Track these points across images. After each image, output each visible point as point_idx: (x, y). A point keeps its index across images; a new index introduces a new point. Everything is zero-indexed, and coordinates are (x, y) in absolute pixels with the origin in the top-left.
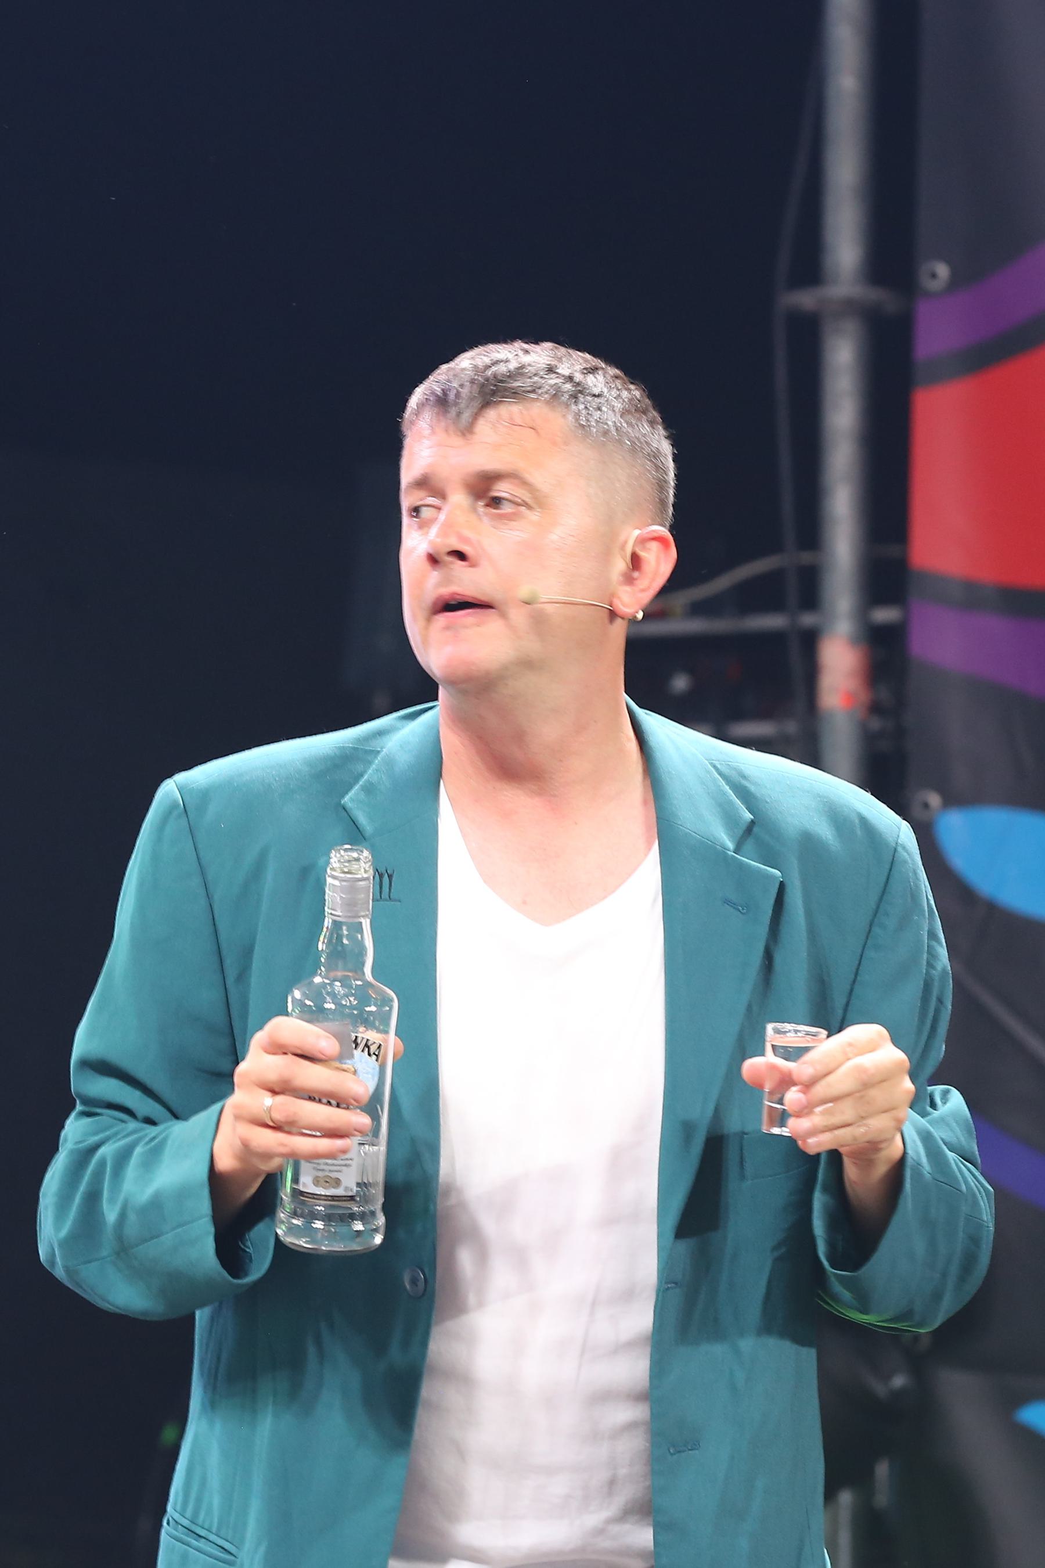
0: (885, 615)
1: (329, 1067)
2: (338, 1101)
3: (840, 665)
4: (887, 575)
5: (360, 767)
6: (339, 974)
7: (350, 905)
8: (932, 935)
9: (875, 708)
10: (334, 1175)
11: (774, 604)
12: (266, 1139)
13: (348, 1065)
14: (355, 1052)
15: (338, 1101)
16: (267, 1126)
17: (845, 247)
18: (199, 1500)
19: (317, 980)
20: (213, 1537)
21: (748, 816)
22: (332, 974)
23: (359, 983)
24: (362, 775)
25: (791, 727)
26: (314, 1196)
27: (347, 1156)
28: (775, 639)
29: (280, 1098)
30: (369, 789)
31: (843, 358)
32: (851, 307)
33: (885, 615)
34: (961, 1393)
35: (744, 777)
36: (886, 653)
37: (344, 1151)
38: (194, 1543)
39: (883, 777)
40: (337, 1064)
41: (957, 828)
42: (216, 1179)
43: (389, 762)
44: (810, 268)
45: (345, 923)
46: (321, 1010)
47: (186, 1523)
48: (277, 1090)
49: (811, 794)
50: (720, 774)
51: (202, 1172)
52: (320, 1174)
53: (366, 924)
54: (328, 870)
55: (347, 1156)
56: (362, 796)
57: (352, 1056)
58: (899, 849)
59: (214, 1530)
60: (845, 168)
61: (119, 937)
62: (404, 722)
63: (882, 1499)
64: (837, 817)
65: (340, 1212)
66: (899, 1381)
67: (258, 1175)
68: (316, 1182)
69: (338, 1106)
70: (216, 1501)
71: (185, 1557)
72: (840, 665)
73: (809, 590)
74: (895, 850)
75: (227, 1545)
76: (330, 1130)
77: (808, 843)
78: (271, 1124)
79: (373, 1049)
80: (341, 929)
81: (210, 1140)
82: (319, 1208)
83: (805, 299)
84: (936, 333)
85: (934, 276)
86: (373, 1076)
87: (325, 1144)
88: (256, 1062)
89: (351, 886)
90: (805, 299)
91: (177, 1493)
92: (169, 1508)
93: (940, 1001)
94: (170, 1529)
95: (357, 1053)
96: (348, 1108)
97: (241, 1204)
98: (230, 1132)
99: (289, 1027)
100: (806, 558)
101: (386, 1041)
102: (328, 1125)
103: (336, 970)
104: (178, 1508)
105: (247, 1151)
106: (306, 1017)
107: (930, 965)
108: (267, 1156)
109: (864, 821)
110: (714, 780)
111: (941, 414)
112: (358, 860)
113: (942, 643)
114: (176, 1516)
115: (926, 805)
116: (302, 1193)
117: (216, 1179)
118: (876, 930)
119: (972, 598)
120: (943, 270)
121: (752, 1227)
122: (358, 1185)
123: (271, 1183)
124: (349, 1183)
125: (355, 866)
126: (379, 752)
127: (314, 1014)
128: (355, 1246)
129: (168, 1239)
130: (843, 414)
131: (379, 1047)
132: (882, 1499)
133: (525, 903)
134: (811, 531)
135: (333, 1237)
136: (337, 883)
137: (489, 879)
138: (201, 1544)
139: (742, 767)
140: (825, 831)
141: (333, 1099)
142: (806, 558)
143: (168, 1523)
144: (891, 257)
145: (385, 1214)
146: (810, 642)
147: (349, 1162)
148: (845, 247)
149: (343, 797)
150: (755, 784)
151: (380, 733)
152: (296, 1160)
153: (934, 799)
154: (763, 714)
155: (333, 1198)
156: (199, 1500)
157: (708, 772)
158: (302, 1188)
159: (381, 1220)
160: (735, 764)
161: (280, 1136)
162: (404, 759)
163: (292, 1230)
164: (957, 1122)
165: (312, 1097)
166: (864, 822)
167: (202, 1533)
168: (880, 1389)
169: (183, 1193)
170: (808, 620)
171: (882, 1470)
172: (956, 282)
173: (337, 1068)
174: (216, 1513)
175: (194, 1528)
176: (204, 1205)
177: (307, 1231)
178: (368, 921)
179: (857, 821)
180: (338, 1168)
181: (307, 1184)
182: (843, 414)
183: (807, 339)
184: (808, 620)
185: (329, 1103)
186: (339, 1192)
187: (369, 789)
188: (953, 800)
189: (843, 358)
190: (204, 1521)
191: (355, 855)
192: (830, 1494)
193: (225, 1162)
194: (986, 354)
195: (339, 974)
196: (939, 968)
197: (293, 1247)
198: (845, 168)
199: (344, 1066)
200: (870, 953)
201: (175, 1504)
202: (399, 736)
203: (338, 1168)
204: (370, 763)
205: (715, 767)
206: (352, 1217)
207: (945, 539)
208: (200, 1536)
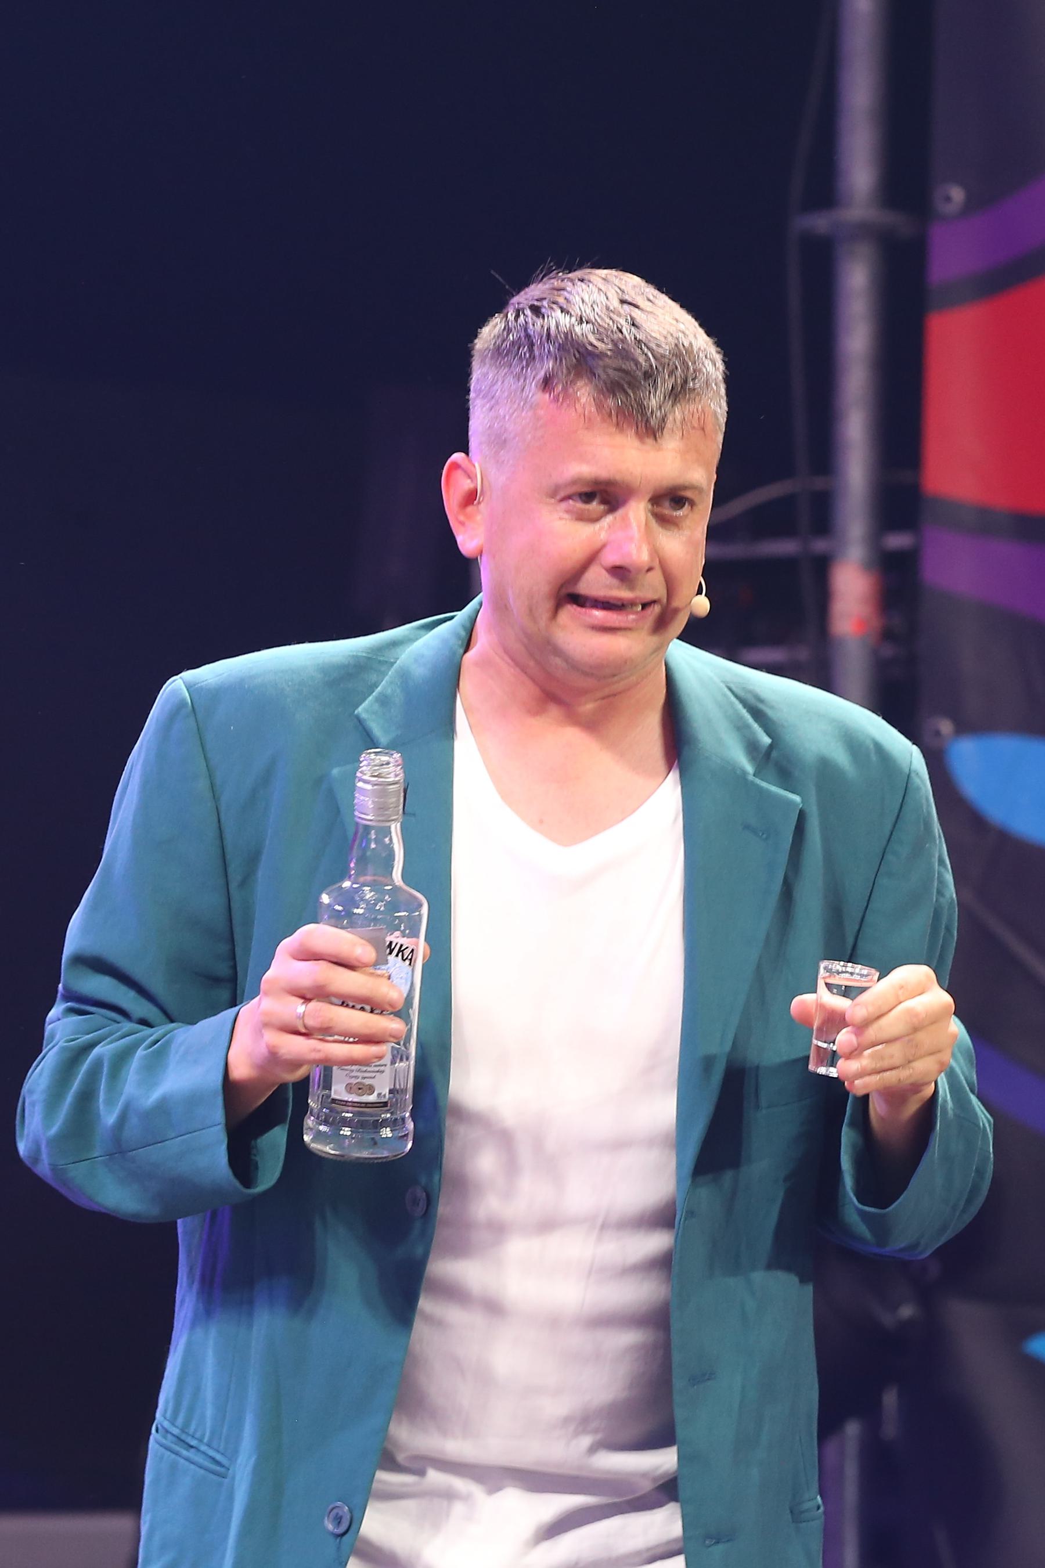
0: (898, 541)
1: (364, 973)
2: (373, 1006)
3: (852, 591)
4: (900, 501)
5: (373, 677)
6: (369, 878)
7: (381, 808)
8: (941, 862)
9: (887, 635)
10: (367, 1082)
11: (785, 529)
12: (295, 1046)
13: (383, 970)
14: (389, 957)
15: (373, 1006)
16: (297, 1033)
17: (860, 171)
18: (191, 1409)
19: (347, 884)
20: (203, 1448)
21: (766, 740)
22: (362, 879)
23: (389, 887)
24: (375, 685)
25: (803, 654)
26: (345, 1103)
27: (382, 1062)
28: (787, 565)
29: (313, 1005)
30: (384, 701)
31: (857, 280)
32: (864, 230)
33: (898, 541)
34: (969, 1323)
35: (762, 701)
36: (898, 580)
37: (380, 1058)
38: (184, 1453)
39: (895, 703)
40: (371, 970)
41: (968, 755)
42: (230, 1087)
43: (404, 676)
44: (824, 189)
45: (373, 827)
46: (350, 915)
47: (176, 1431)
48: (308, 996)
49: (827, 718)
50: (736, 696)
51: (216, 1079)
52: (354, 1081)
53: (395, 828)
54: (358, 774)
55: (382, 1062)
56: (376, 707)
57: (386, 962)
58: (913, 775)
59: (206, 1440)
60: (860, 91)
61: (114, 849)
62: (422, 632)
63: (890, 1429)
64: (853, 742)
65: (368, 1120)
66: (906, 1312)
67: (273, 1085)
68: (349, 1088)
69: (372, 1012)
70: (209, 1412)
71: (174, 1467)
72: (852, 591)
73: (822, 515)
74: (909, 776)
75: (218, 1457)
76: (366, 1036)
77: (825, 765)
78: (303, 1030)
79: (407, 953)
80: (369, 833)
81: (225, 1051)
82: (347, 1115)
83: (820, 223)
84: (951, 257)
85: (948, 199)
86: (406, 980)
87: (359, 1050)
88: (284, 967)
89: (382, 789)
90: (820, 223)
91: (167, 1402)
92: (158, 1415)
93: (948, 929)
94: (159, 1437)
95: (391, 958)
96: (381, 1013)
97: (262, 1108)
98: (251, 1037)
99: (318, 934)
100: (819, 483)
101: (417, 945)
102: (365, 1031)
103: (365, 875)
104: (168, 1415)
105: (273, 1057)
106: (333, 921)
107: (940, 893)
108: (295, 1064)
109: (879, 748)
110: (732, 704)
111: (957, 343)
112: (388, 763)
113: (956, 569)
114: (166, 1424)
115: (938, 733)
116: (334, 1101)
117: (230, 1087)
118: (889, 857)
119: (984, 524)
120: (957, 194)
121: (769, 1149)
122: (391, 1092)
123: (302, 1087)
124: (382, 1088)
125: (384, 770)
126: (392, 664)
127: (343, 919)
128: (384, 1153)
129: (173, 1146)
130: (857, 339)
131: (413, 951)
132: (890, 1429)
133: (541, 822)
134: (824, 454)
135: (360, 1144)
136: (369, 787)
137: (507, 797)
138: (190, 1454)
139: (758, 690)
140: (841, 757)
141: (368, 1004)
142: (819, 483)
143: (157, 1431)
144: (906, 179)
145: (413, 1120)
146: (822, 568)
147: (382, 1068)
148: (860, 171)
149: (357, 707)
150: (772, 707)
151: (394, 644)
152: (327, 1067)
153: (946, 727)
154: (775, 640)
155: (361, 1104)
156: (191, 1409)
157: (725, 695)
158: (333, 1096)
159: (410, 1125)
160: (751, 687)
161: (312, 1043)
162: (419, 672)
163: (319, 1136)
164: (961, 1053)
165: (345, 1001)
166: (879, 749)
167: (193, 1443)
168: (887, 1320)
169: (194, 1099)
170: (820, 546)
171: (890, 1399)
172: (971, 205)
173: (372, 974)
174: (209, 1424)
175: (183, 1437)
176: (218, 1114)
177: (334, 1137)
178: (399, 825)
179: (872, 746)
180: (373, 1075)
181: (339, 1091)
182: (857, 339)
183: (821, 263)
184: (820, 546)
185: (362, 1009)
186: (372, 1098)
187: (384, 701)
188: (965, 727)
189: (857, 280)
190: (196, 1430)
191: (385, 758)
192: (828, 1425)
193: (241, 1070)
194: (999, 280)
195: (369, 878)
196: (948, 896)
197: (320, 1154)
198: (860, 91)
199: (379, 972)
200: (883, 881)
201: (166, 1411)
202: (418, 645)
203: (373, 1075)
204: (385, 674)
205: (730, 689)
206: (385, 1123)
207: (959, 464)
208: (192, 1447)
